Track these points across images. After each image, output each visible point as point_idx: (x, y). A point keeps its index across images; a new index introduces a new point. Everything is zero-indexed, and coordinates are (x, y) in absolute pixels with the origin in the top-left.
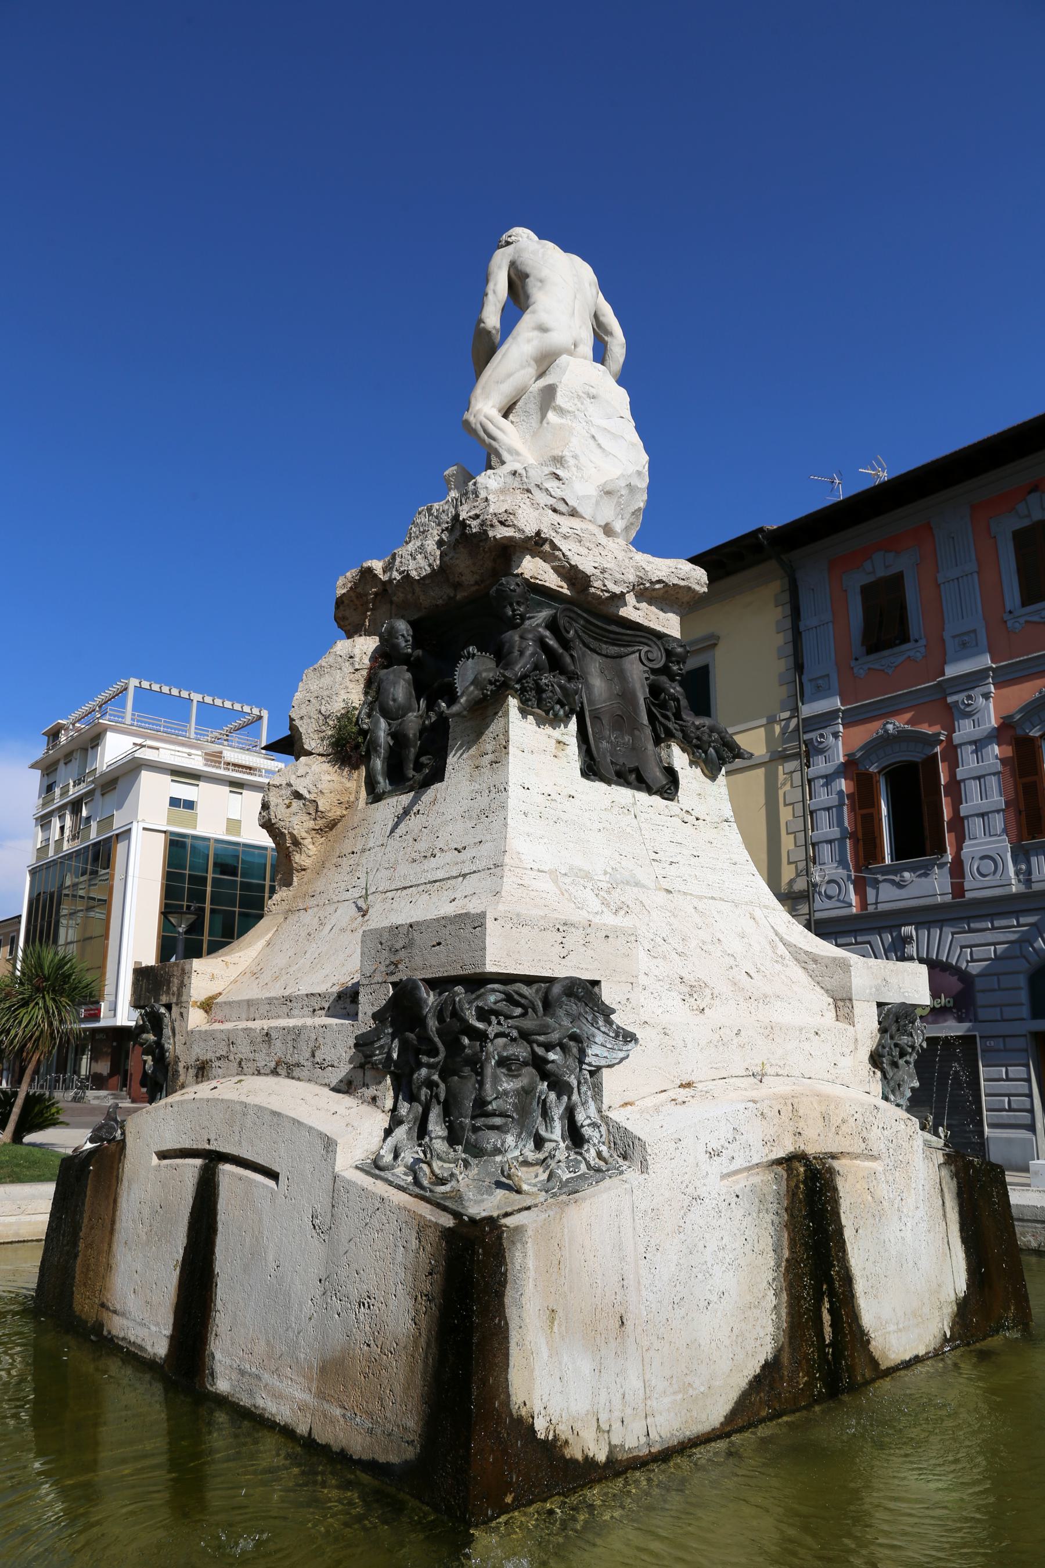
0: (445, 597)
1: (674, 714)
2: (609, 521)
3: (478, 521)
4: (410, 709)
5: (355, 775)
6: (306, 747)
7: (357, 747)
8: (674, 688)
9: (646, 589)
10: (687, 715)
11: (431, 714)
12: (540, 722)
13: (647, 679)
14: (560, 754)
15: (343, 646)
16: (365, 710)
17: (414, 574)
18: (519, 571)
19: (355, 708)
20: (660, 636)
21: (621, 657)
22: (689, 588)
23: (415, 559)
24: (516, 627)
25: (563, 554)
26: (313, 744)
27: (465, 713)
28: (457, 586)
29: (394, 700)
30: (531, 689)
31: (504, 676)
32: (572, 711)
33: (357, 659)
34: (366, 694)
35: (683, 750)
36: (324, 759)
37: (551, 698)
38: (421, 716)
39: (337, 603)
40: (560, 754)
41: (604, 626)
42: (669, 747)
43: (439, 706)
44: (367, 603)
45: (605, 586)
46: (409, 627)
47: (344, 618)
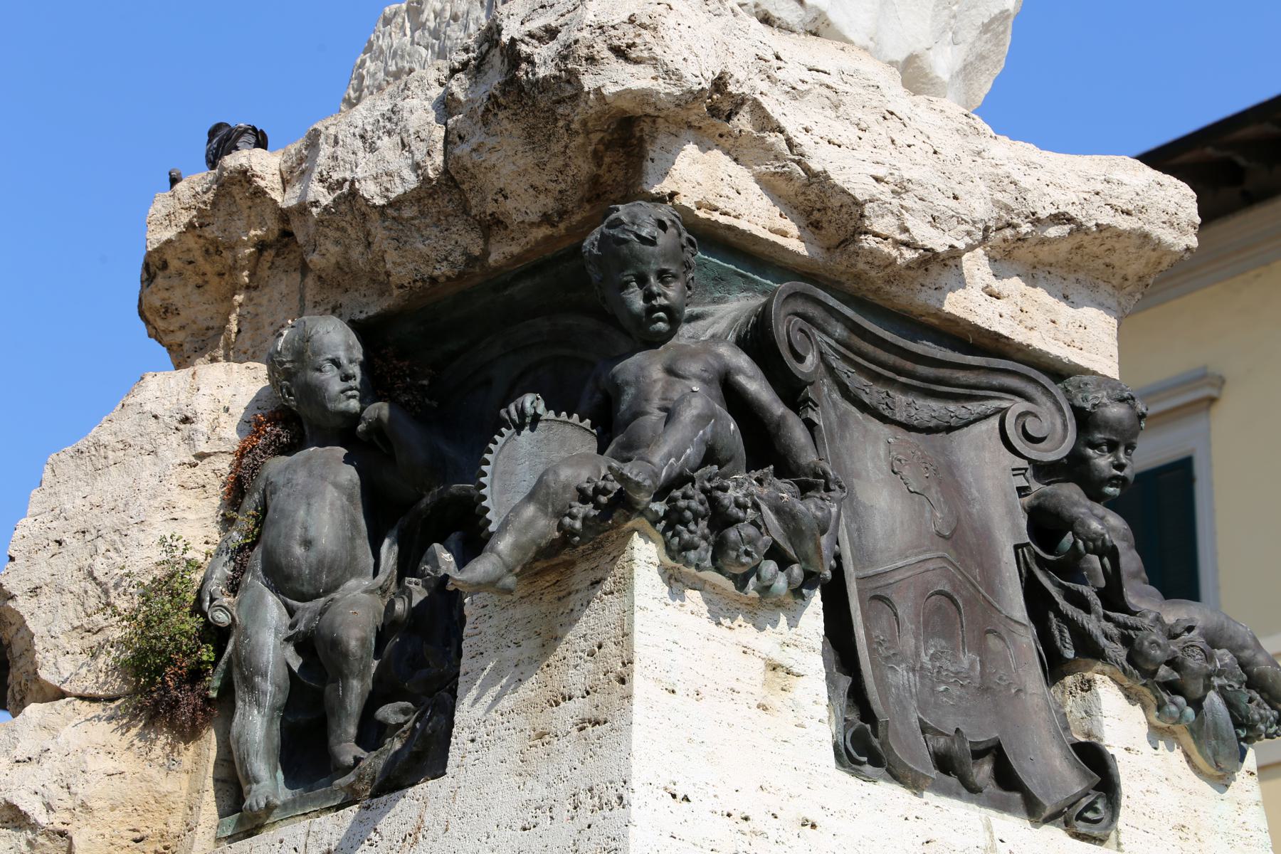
0: (457, 257)
1: (1100, 593)
2: (918, 48)
3: (554, 46)
4: (351, 569)
5: (188, 754)
6: (43, 674)
7: (196, 674)
8: (1101, 519)
9: (1021, 239)
10: (1140, 595)
11: (410, 582)
12: (720, 611)
13: (1022, 491)
14: (775, 700)
15: (164, 388)
16: (223, 571)
17: (370, 190)
18: (665, 187)
19: (192, 565)
20: (1058, 372)
21: (950, 429)
22: (1146, 236)
23: (373, 149)
24: (654, 342)
25: (789, 142)
26: (67, 667)
27: (510, 581)
28: (491, 226)
29: (307, 543)
30: (697, 516)
31: (621, 478)
32: (811, 579)
33: (202, 426)
34: (227, 523)
35: (1130, 696)
36: (97, 708)
37: (751, 542)
38: (383, 590)
39: (147, 267)
40: (775, 700)
41: (902, 342)
42: (1088, 686)
43: (435, 561)
44: (234, 268)
45: (906, 230)
46: (353, 338)
47: (167, 311)
